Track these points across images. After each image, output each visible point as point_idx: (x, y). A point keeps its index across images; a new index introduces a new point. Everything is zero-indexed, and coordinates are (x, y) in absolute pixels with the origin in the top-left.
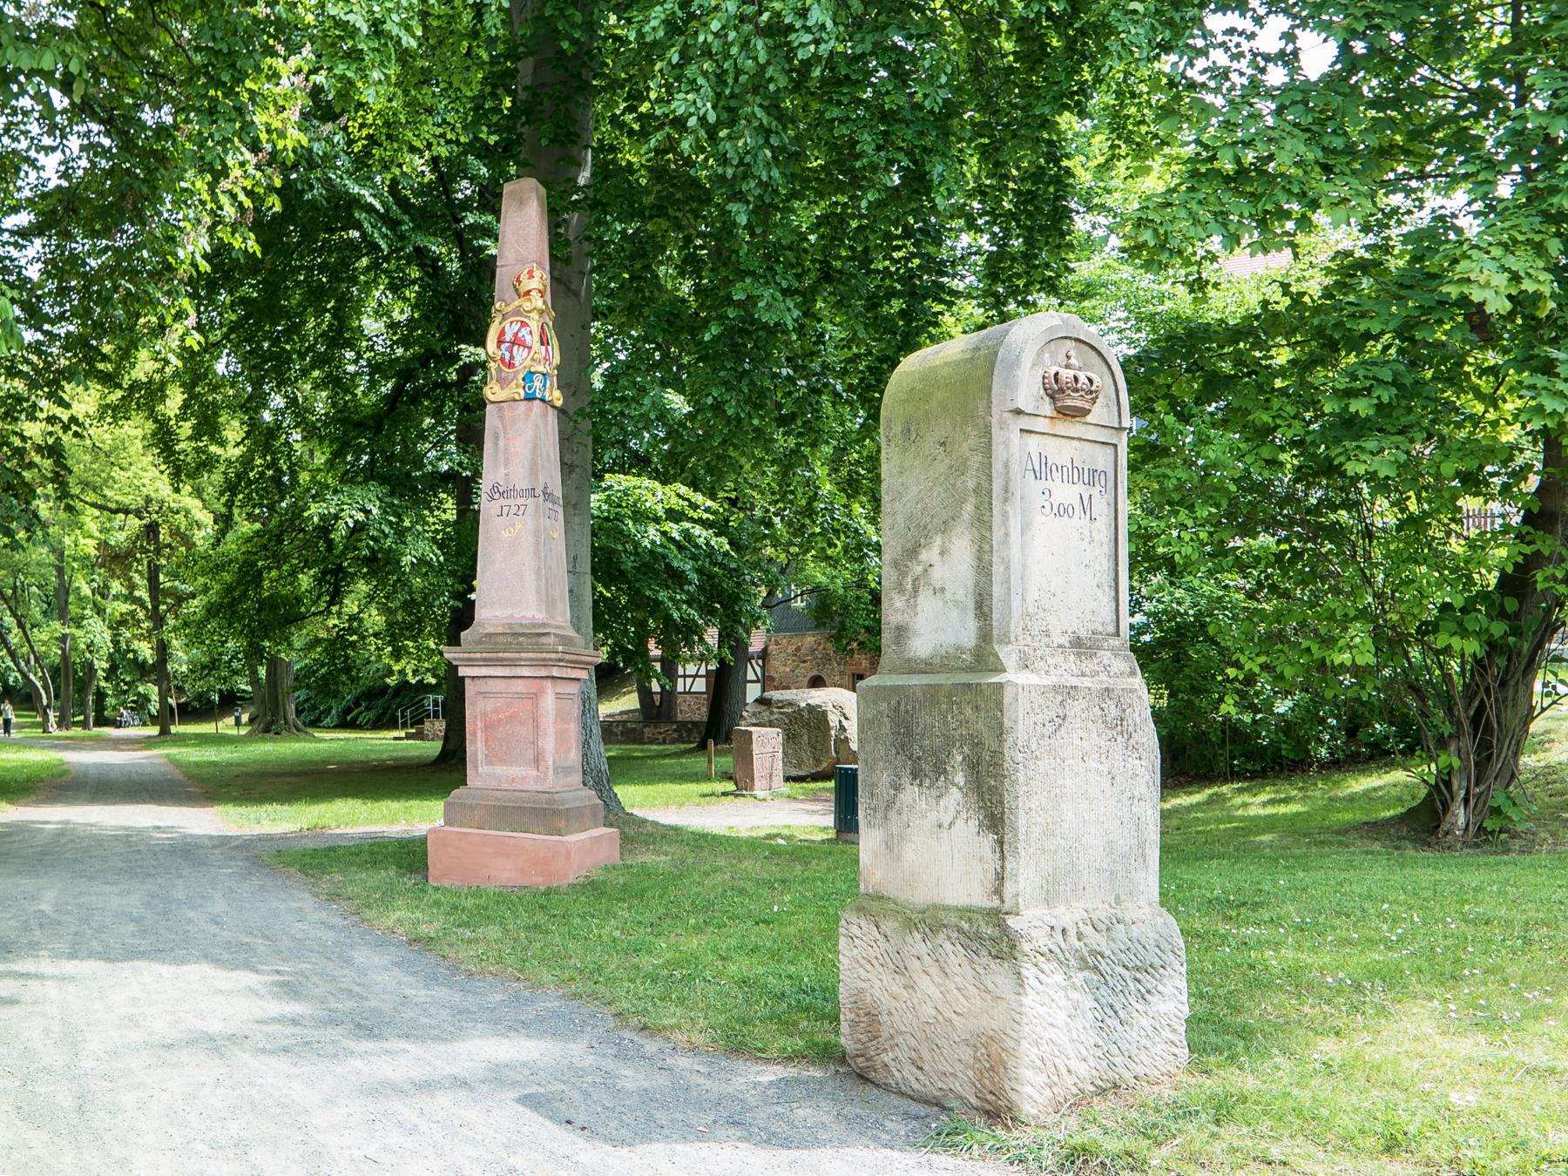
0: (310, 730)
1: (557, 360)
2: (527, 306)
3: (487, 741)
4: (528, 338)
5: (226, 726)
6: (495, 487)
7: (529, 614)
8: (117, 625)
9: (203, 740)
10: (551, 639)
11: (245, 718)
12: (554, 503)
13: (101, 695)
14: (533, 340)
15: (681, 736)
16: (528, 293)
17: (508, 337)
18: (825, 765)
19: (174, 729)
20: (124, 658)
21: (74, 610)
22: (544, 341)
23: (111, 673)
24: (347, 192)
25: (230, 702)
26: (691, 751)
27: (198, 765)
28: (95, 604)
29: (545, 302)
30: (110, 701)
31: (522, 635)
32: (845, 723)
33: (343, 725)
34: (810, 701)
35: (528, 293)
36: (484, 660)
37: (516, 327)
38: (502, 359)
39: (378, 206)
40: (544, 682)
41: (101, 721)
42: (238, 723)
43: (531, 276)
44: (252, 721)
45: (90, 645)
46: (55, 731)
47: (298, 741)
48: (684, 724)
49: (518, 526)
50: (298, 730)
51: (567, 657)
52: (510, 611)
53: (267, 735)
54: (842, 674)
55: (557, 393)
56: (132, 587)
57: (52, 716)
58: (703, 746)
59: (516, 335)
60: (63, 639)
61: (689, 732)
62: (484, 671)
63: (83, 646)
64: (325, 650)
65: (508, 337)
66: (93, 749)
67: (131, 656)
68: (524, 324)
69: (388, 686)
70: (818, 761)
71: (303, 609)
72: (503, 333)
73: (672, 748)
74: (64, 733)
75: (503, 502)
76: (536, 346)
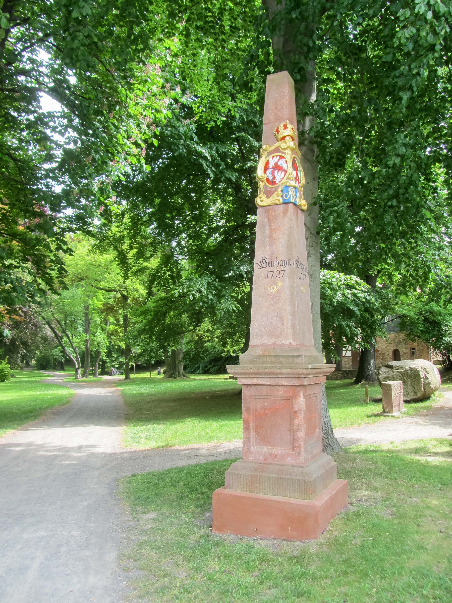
0: (188, 375)
1: (303, 181)
2: (282, 145)
3: (257, 428)
4: (284, 166)
5: (154, 374)
6: (263, 260)
7: (287, 342)
8: (110, 335)
9: (143, 381)
10: (303, 360)
11: (162, 370)
12: (303, 269)
13: (104, 362)
14: (288, 166)
15: (344, 376)
16: (284, 138)
17: (271, 165)
18: (419, 395)
19: (131, 376)
20: (113, 347)
21: (92, 329)
22: (295, 168)
23: (109, 354)
24: (196, 150)
25: (158, 364)
26: (351, 384)
27: (134, 396)
28: (102, 327)
29: (294, 144)
30: (108, 365)
31: (282, 356)
32: (427, 376)
33: (206, 372)
34: (411, 366)
35: (284, 138)
36: (255, 374)
37: (276, 159)
38: (268, 180)
39: (209, 158)
40: (298, 389)
41: (104, 373)
42: (159, 373)
43: (285, 127)
44: (164, 373)
45: (99, 343)
46: (81, 378)
47: (183, 381)
48: (345, 371)
49: (279, 284)
50: (184, 376)
51: (314, 371)
52: (274, 340)
53: (170, 379)
54: (406, 348)
55: (303, 202)
56: (117, 320)
57: (80, 372)
58: (357, 382)
59: (276, 164)
60: (86, 341)
61: (347, 374)
62: (255, 381)
63: (96, 344)
64: (194, 344)
65: (271, 165)
66: (92, 387)
67: (116, 347)
68: (282, 157)
69: (222, 357)
70: (415, 393)
71: (184, 329)
72: (267, 163)
73: (341, 382)
74: (84, 379)
75: (268, 269)
76: (290, 170)
